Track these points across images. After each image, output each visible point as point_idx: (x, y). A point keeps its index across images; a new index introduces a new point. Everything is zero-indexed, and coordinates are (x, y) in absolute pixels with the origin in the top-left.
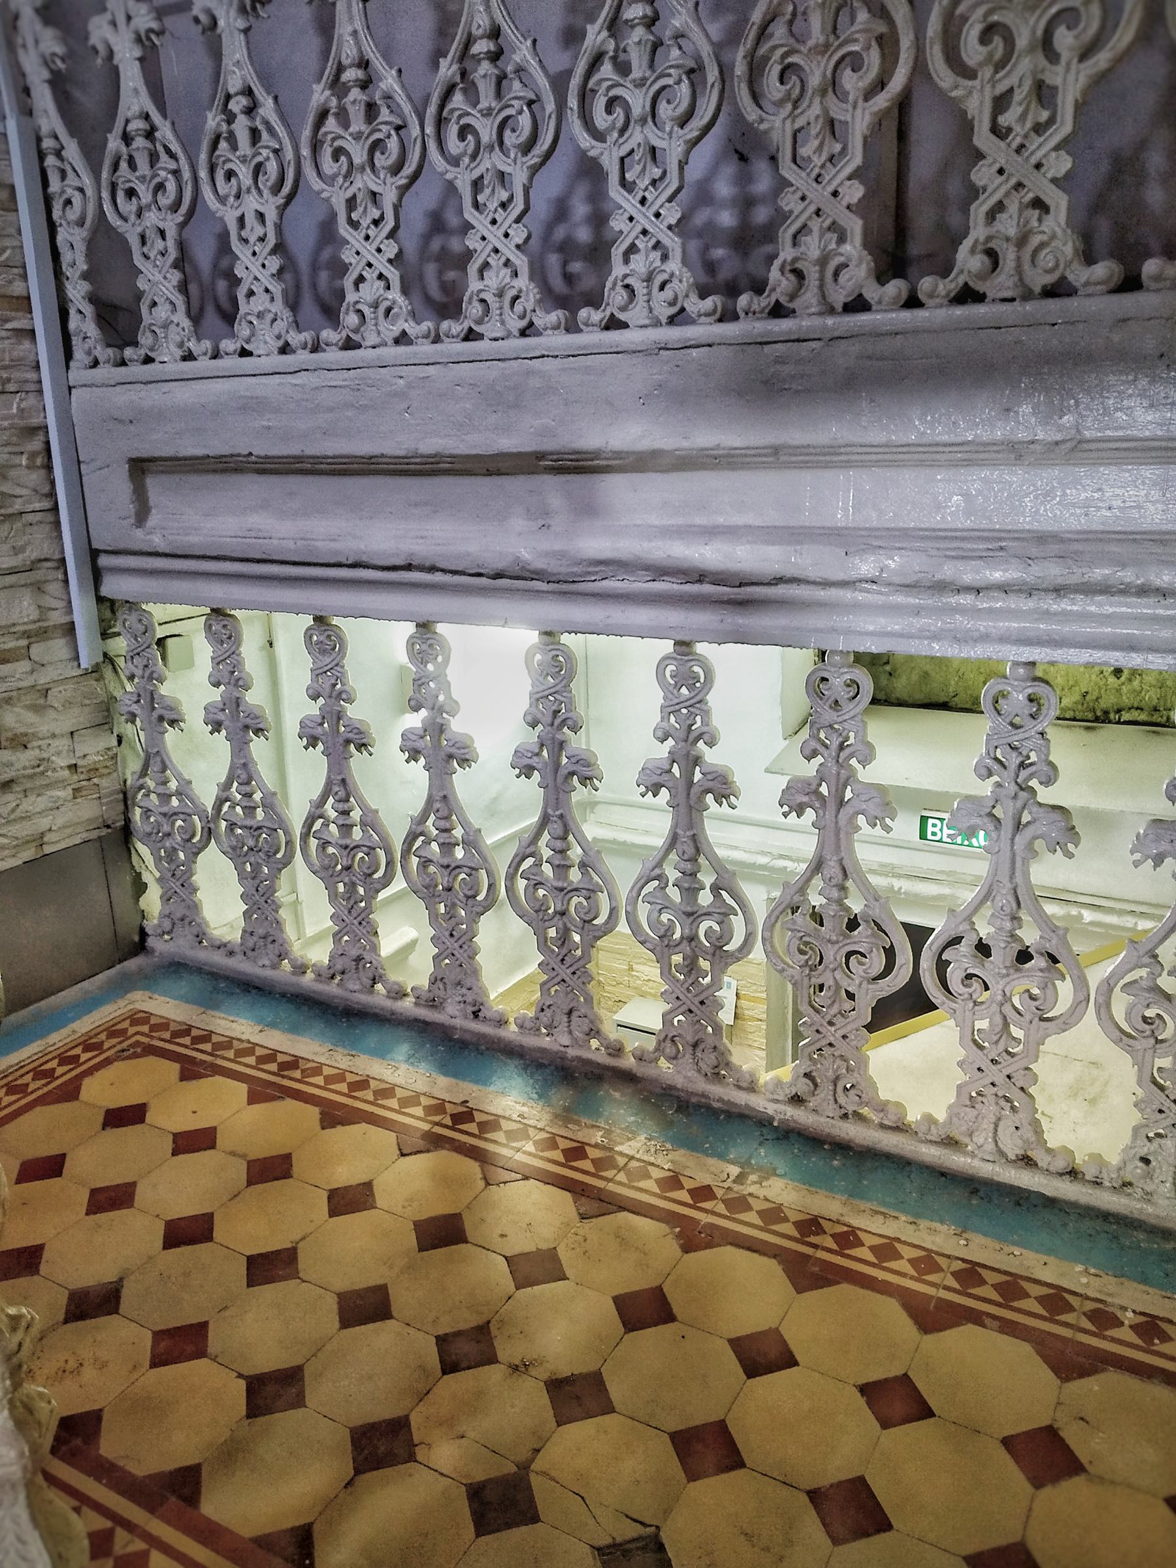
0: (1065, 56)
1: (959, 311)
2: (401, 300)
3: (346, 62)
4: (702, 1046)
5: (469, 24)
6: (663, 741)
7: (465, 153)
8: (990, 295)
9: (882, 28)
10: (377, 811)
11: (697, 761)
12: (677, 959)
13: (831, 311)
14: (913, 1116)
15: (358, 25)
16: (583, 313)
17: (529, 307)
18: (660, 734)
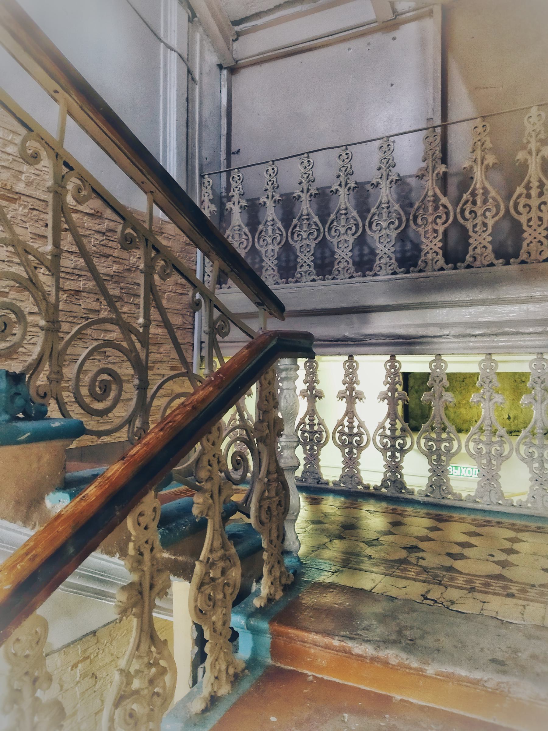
0: (489, 217)
1: (468, 270)
2: (314, 271)
3: (383, 201)
4: (397, 482)
5: (302, 212)
6: (306, 384)
7: (423, 224)
8: (475, 266)
9: (446, 210)
10: (364, 422)
11: (353, 389)
12: (435, 457)
13: (435, 271)
14: (464, 495)
15: (308, 206)
16: (459, 264)
17: (352, 271)
18: (385, 383)
